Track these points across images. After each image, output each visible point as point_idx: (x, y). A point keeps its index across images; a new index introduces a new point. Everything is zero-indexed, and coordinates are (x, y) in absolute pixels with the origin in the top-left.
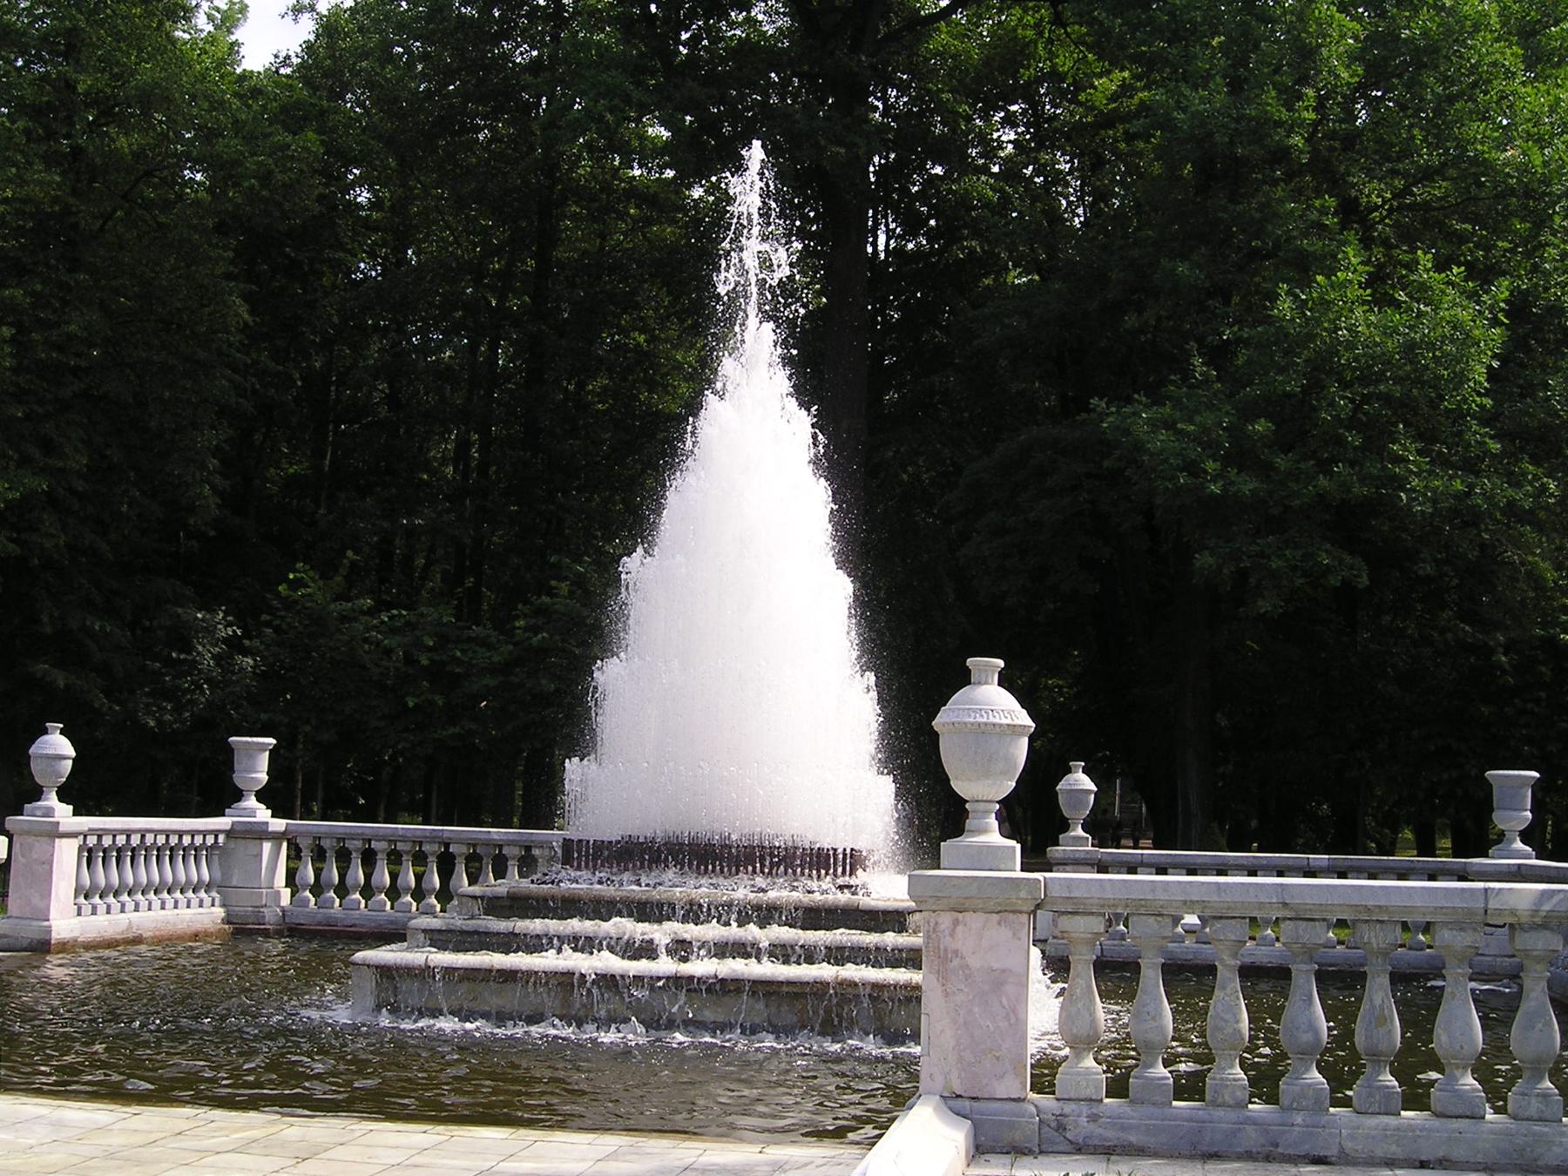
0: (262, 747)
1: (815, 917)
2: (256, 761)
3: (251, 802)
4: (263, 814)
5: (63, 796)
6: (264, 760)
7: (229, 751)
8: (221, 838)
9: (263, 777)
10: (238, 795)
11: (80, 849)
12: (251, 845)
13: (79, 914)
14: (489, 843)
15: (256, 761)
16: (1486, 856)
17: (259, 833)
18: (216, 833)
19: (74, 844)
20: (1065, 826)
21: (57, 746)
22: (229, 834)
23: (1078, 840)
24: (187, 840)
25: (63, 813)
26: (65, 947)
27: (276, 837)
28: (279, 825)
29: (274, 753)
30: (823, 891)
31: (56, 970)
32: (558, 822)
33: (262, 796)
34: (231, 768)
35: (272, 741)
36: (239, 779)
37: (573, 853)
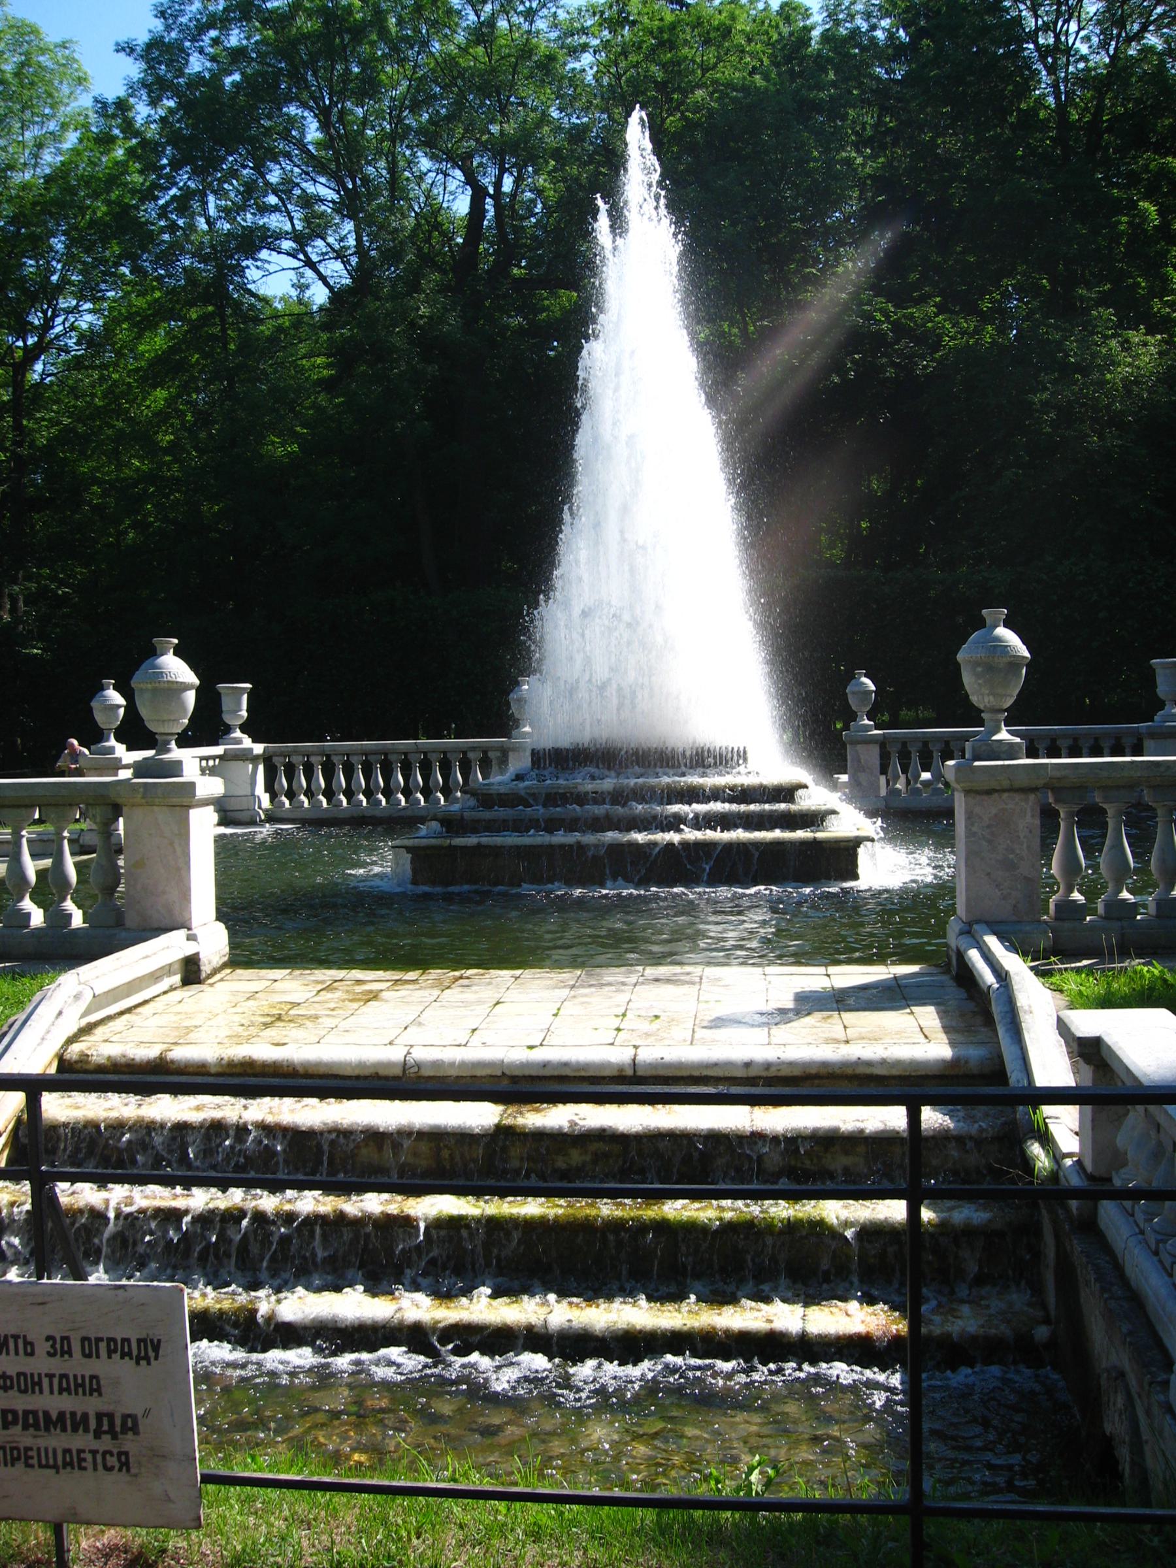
3: (238, 734)
4: (247, 742)
10: (228, 729)
17: (245, 756)
18: (214, 758)
28: (259, 748)
29: (252, 695)
33: (244, 728)
34: (220, 711)
35: (249, 686)
36: (228, 719)
37: (539, 758)
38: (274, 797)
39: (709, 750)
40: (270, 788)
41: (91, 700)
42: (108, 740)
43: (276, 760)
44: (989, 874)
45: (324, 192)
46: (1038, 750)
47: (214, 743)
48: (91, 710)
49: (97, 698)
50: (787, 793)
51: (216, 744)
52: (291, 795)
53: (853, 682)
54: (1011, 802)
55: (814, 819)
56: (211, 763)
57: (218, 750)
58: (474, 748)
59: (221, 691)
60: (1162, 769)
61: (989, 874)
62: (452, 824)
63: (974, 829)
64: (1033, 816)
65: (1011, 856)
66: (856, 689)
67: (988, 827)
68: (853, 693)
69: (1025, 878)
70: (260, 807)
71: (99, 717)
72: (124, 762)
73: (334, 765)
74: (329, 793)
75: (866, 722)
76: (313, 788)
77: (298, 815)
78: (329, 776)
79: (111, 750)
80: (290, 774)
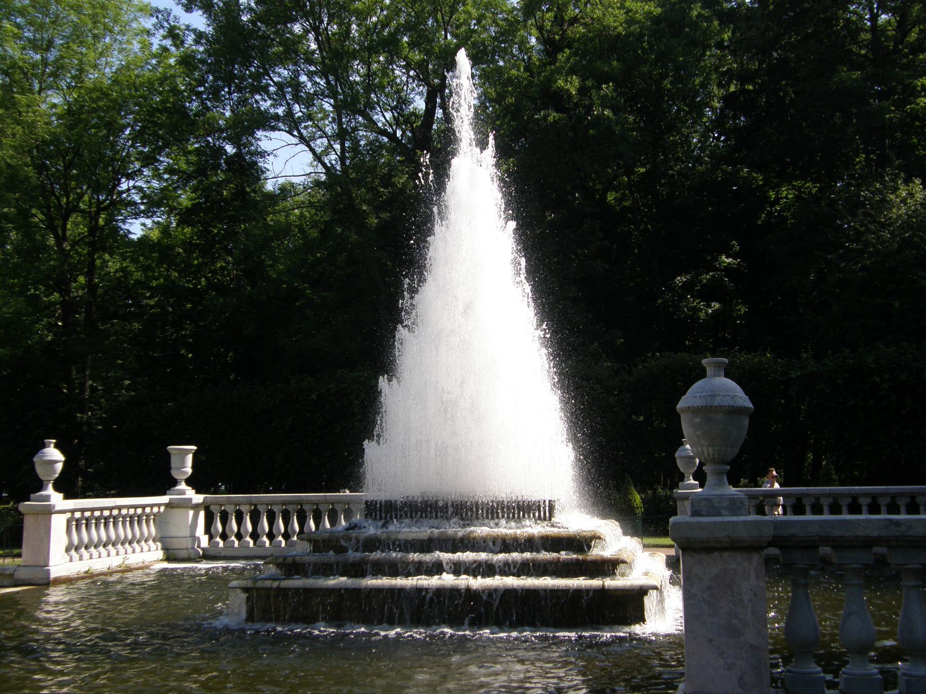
0: (189, 451)
1: (529, 544)
2: (184, 458)
3: (183, 486)
4: (190, 493)
5: (58, 487)
6: (189, 459)
7: (168, 455)
8: (162, 509)
9: (189, 470)
10: (175, 482)
11: (69, 522)
12: (184, 510)
13: (71, 561)
14: (310, 502)
15: (184, 458)
16: (29, 500)
17: (187, 504)
18: (159, 505)
19: (64, 518)
20: (682, 477)
21: (54, 454)
22: (167, 505)
23: (692, 487)
24: (148, 510)
25: (57, 499)
26: (59, 581)
27: (196, 507)
28: (198, 498)
29: (196, 455)
30: (533, 528)
31: (56, 595)
32: (361, 487)
33: (189, 482)
34: (169, 469)
35: (194, 448)
36: (175, 474)
37: (374, 510)
38: (211, 538)
39: (462, 505)
40: (208, 530)
41: (34, 456)
42: (46, 489)
43: (212, 508)
44: (710, 640)
45: (322, 83)
46: (898, 507)
47: (163, 493)
48: (33, 464)
49: (39, 454)
50: (579, 543)
51: (164, 494)
52: (224, 536)
53: (681, 448)
54: (733, 562)
55: (608, 567)
56: (155, 510)
57: (165, 499)
58: (882, 495)
59: (170, 451)
60: (903, 528)
61: (710, 640)
62: (291, 567)
63: (694, 591)
64: (757, 578)
65: (734, 621)
66: (683, 454)
67: (709, 588)
68: (681, 457)
69: (751, 646)
70: (199, 546)
71: (40, 471)
72: (57, 509)
73: (260, 512)
74: (255, 536)
75: (692, 481)
76: (242, 531)
77: (259, 552)
78: (255, 522)
79: (47, 498)
80: (224, 522)
